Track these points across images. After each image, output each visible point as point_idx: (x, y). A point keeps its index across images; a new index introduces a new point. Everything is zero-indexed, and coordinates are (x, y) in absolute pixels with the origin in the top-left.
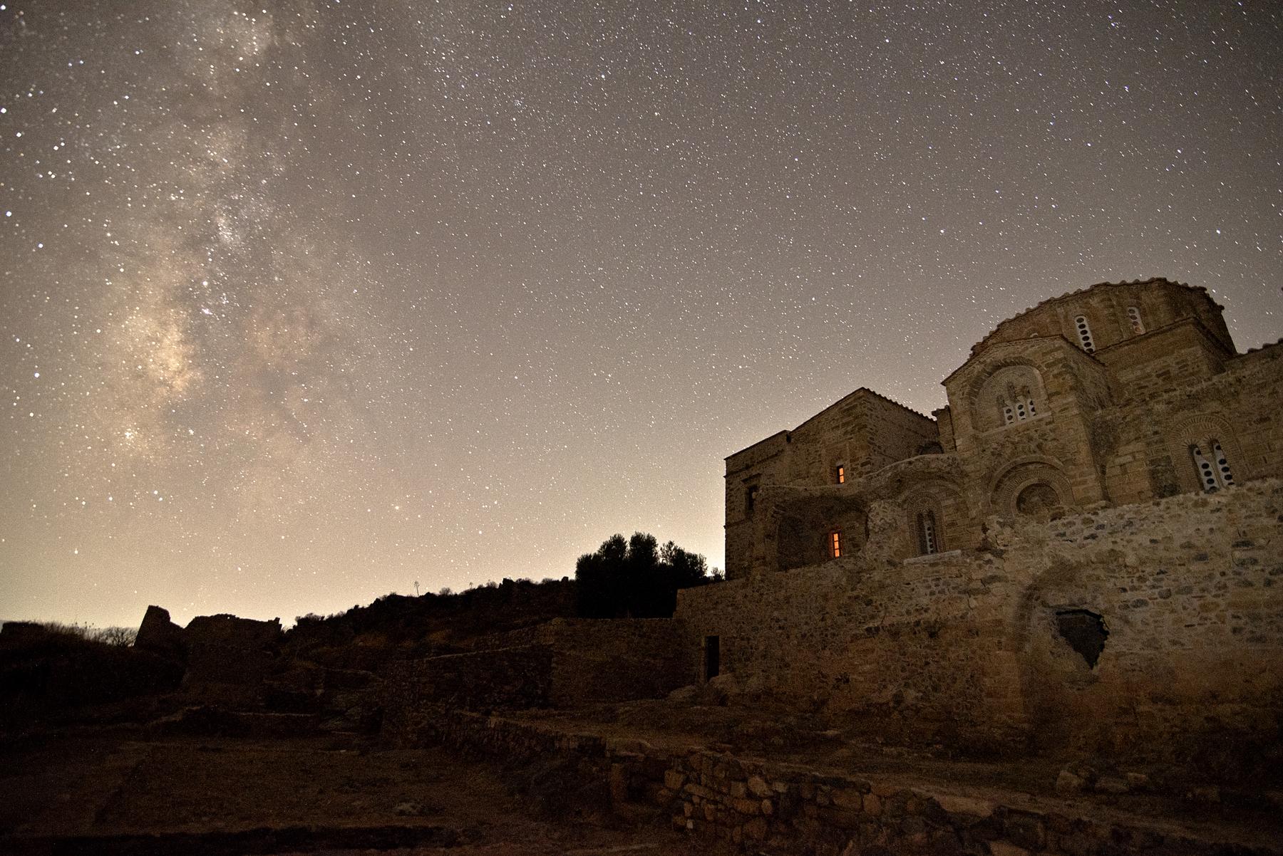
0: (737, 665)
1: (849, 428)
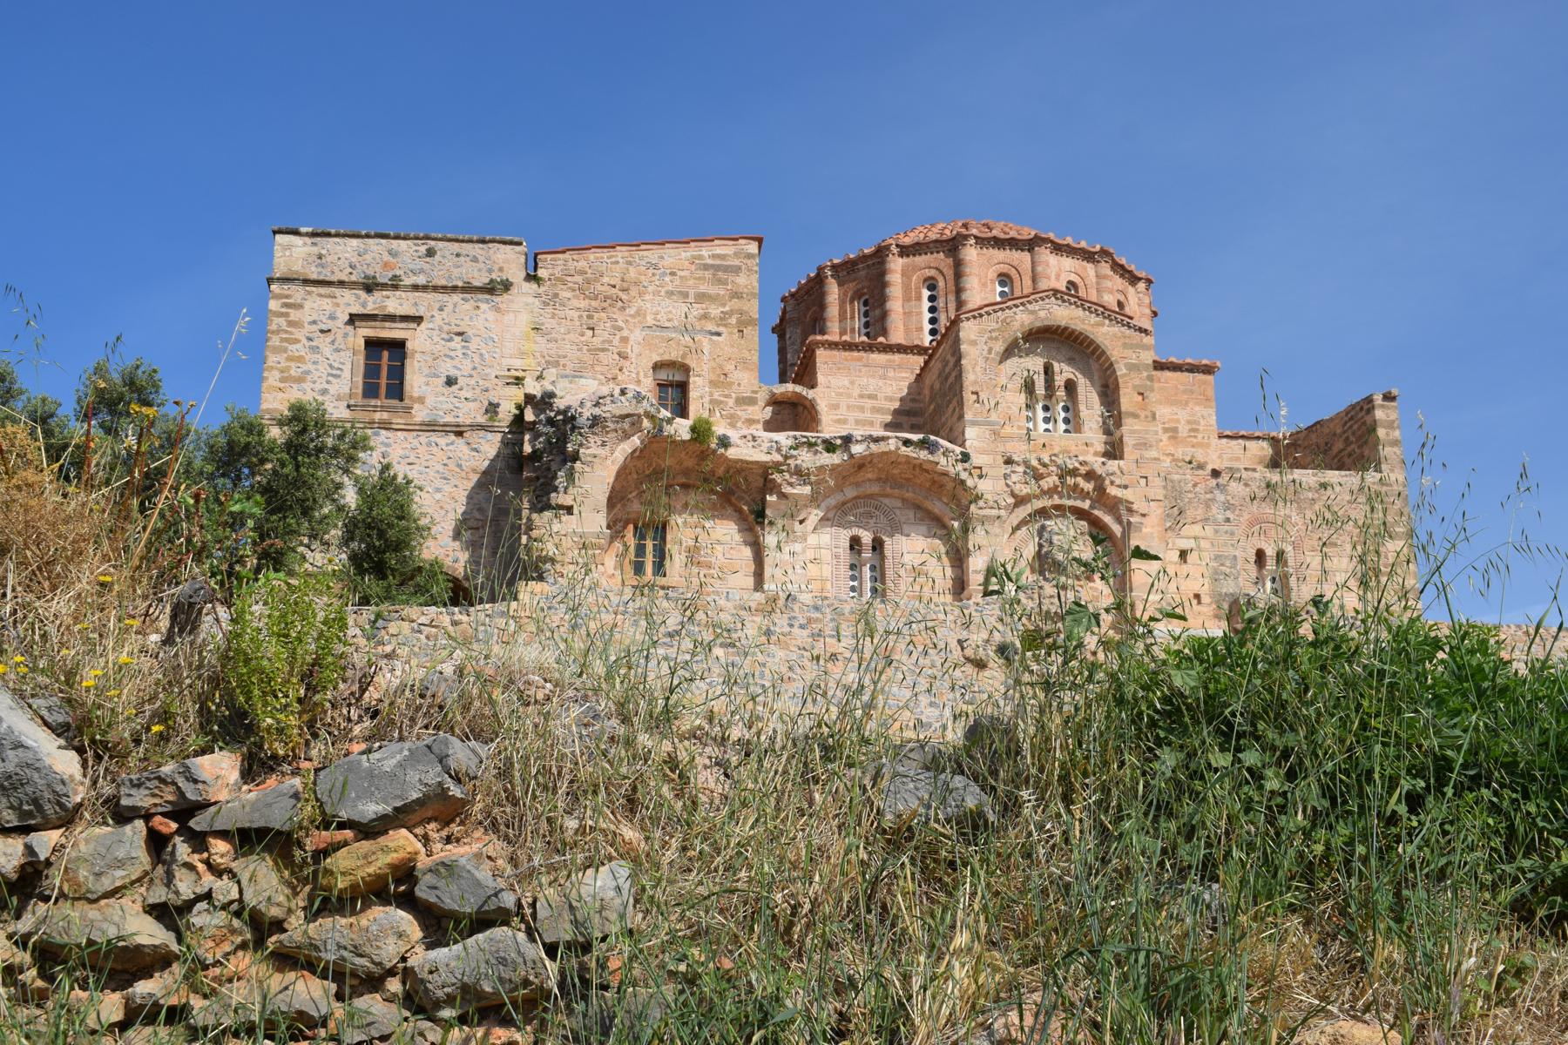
1: (715, 311)
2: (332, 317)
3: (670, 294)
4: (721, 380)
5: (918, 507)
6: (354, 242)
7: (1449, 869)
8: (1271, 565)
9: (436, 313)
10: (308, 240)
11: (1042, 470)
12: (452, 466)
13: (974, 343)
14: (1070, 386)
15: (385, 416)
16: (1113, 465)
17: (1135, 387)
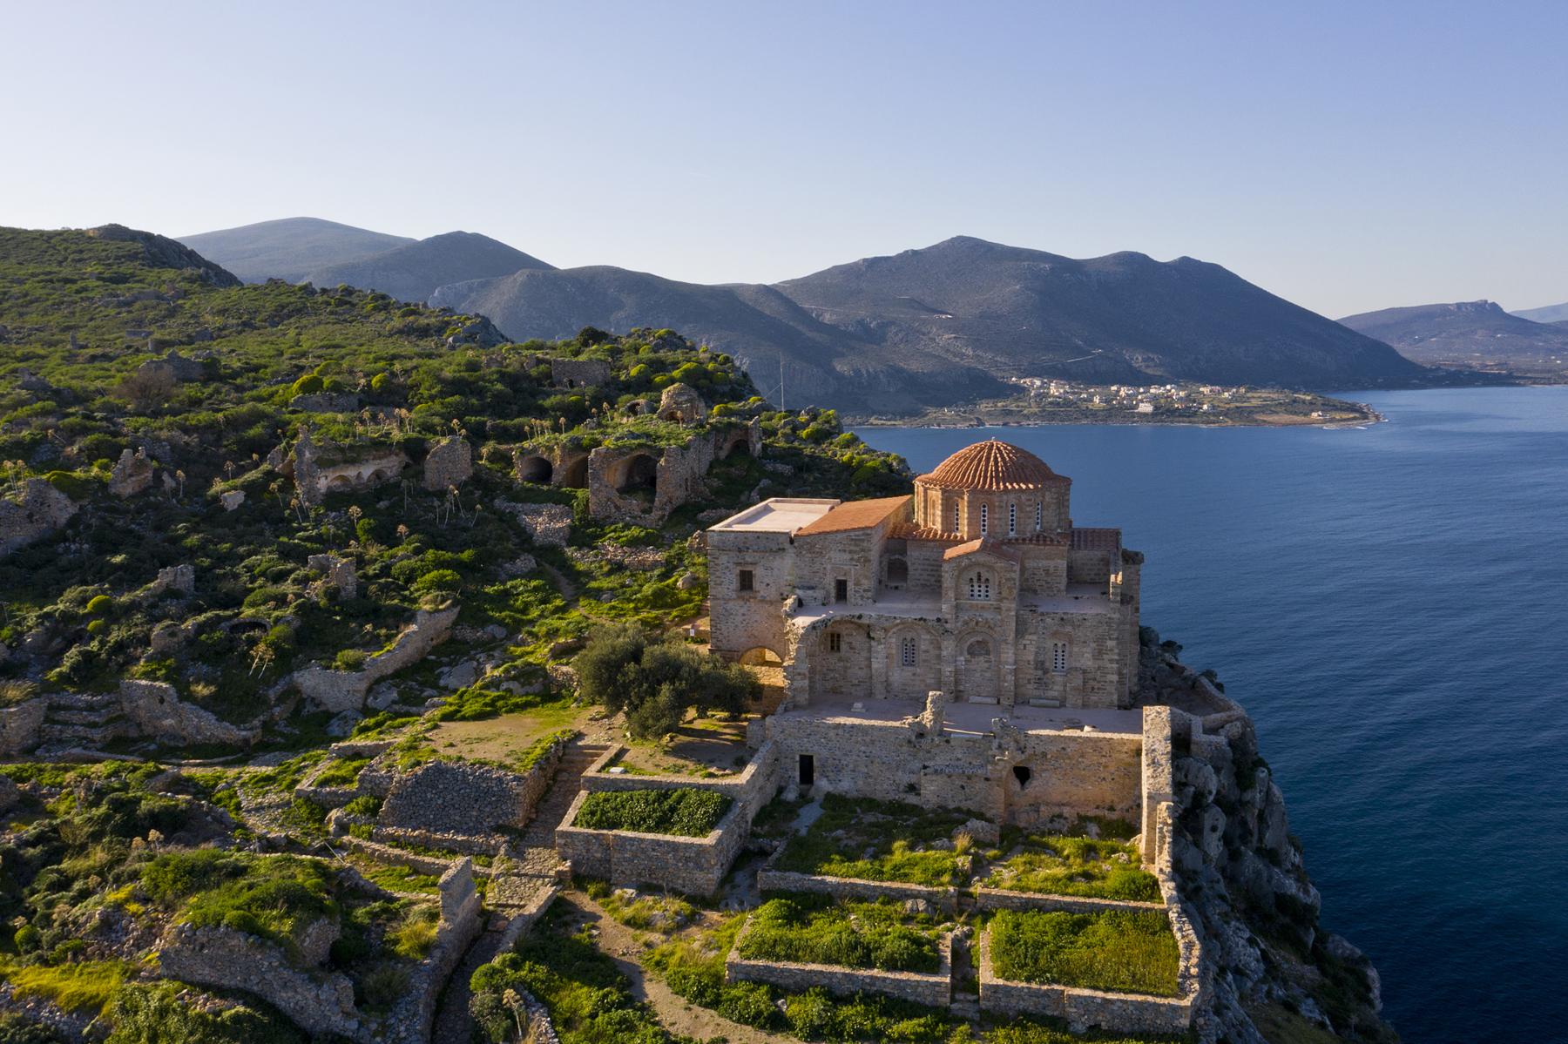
4: (857, 584)
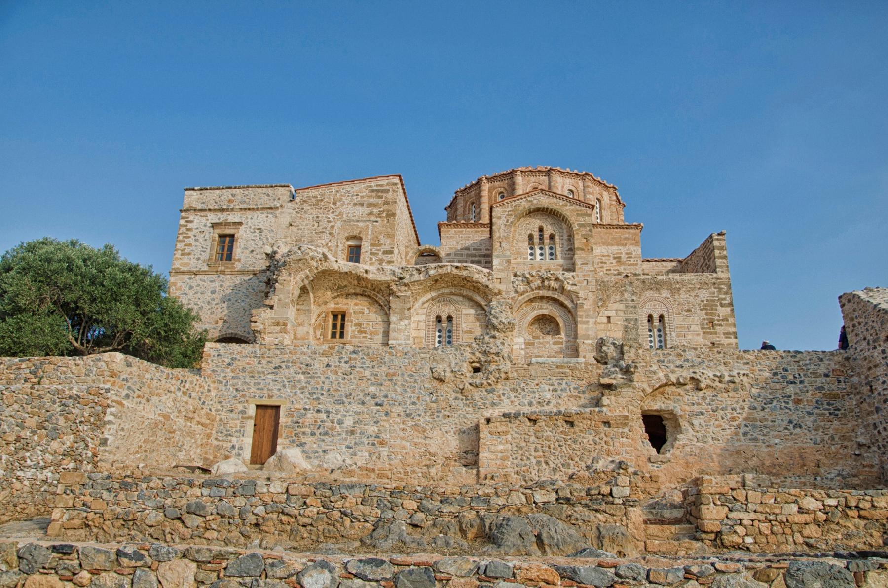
0: (308, 439)
1: (376, 211)
2: (205, 226)
3: (355, 204)
5: (470, 299)
6: (218, 192)
7: (256, 560)
8: (656, 323)
9: (249, 220)
10: (199, 192)
11: (531, 278)
12: (250, 290)
13: (499, 218)
14: (552, 237)
15: (223, 268)
16: (569, 275)
17: (582, 235)
